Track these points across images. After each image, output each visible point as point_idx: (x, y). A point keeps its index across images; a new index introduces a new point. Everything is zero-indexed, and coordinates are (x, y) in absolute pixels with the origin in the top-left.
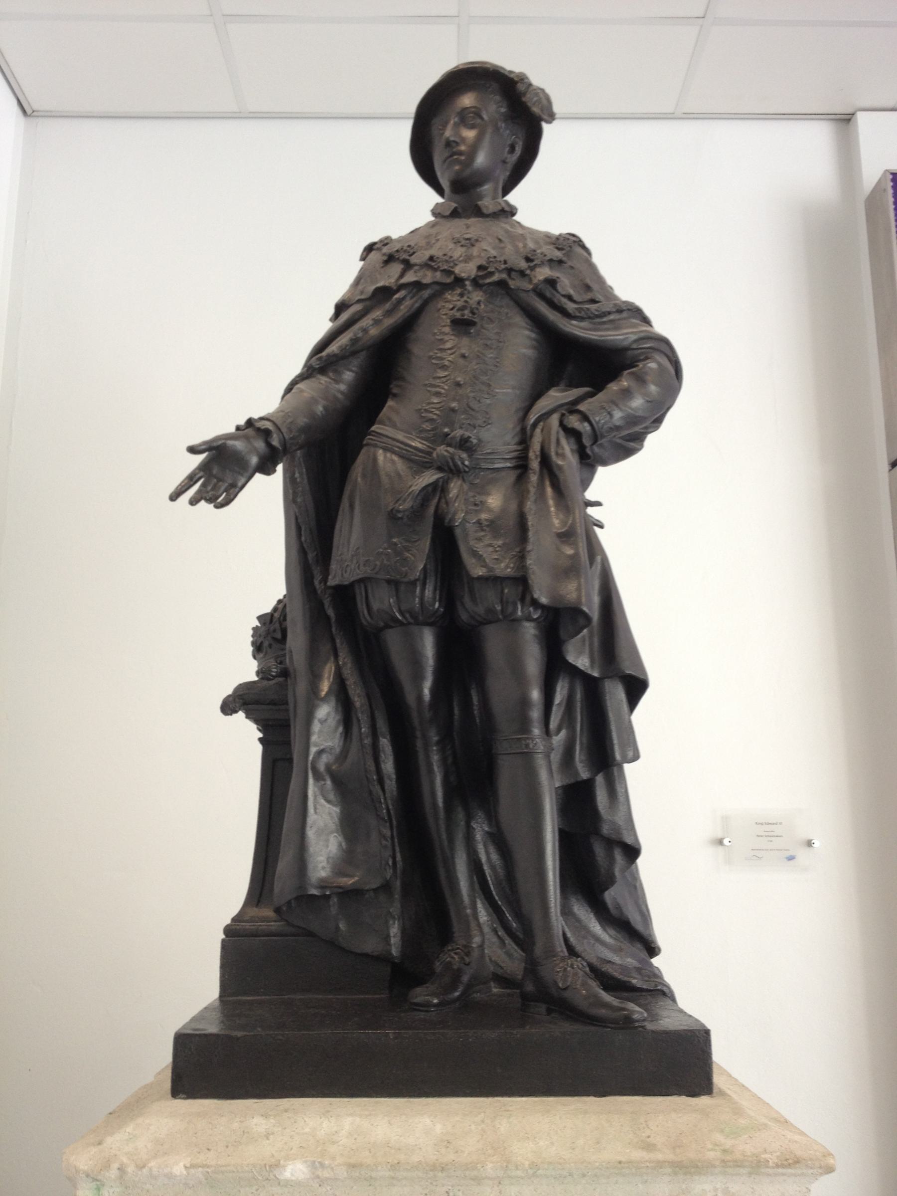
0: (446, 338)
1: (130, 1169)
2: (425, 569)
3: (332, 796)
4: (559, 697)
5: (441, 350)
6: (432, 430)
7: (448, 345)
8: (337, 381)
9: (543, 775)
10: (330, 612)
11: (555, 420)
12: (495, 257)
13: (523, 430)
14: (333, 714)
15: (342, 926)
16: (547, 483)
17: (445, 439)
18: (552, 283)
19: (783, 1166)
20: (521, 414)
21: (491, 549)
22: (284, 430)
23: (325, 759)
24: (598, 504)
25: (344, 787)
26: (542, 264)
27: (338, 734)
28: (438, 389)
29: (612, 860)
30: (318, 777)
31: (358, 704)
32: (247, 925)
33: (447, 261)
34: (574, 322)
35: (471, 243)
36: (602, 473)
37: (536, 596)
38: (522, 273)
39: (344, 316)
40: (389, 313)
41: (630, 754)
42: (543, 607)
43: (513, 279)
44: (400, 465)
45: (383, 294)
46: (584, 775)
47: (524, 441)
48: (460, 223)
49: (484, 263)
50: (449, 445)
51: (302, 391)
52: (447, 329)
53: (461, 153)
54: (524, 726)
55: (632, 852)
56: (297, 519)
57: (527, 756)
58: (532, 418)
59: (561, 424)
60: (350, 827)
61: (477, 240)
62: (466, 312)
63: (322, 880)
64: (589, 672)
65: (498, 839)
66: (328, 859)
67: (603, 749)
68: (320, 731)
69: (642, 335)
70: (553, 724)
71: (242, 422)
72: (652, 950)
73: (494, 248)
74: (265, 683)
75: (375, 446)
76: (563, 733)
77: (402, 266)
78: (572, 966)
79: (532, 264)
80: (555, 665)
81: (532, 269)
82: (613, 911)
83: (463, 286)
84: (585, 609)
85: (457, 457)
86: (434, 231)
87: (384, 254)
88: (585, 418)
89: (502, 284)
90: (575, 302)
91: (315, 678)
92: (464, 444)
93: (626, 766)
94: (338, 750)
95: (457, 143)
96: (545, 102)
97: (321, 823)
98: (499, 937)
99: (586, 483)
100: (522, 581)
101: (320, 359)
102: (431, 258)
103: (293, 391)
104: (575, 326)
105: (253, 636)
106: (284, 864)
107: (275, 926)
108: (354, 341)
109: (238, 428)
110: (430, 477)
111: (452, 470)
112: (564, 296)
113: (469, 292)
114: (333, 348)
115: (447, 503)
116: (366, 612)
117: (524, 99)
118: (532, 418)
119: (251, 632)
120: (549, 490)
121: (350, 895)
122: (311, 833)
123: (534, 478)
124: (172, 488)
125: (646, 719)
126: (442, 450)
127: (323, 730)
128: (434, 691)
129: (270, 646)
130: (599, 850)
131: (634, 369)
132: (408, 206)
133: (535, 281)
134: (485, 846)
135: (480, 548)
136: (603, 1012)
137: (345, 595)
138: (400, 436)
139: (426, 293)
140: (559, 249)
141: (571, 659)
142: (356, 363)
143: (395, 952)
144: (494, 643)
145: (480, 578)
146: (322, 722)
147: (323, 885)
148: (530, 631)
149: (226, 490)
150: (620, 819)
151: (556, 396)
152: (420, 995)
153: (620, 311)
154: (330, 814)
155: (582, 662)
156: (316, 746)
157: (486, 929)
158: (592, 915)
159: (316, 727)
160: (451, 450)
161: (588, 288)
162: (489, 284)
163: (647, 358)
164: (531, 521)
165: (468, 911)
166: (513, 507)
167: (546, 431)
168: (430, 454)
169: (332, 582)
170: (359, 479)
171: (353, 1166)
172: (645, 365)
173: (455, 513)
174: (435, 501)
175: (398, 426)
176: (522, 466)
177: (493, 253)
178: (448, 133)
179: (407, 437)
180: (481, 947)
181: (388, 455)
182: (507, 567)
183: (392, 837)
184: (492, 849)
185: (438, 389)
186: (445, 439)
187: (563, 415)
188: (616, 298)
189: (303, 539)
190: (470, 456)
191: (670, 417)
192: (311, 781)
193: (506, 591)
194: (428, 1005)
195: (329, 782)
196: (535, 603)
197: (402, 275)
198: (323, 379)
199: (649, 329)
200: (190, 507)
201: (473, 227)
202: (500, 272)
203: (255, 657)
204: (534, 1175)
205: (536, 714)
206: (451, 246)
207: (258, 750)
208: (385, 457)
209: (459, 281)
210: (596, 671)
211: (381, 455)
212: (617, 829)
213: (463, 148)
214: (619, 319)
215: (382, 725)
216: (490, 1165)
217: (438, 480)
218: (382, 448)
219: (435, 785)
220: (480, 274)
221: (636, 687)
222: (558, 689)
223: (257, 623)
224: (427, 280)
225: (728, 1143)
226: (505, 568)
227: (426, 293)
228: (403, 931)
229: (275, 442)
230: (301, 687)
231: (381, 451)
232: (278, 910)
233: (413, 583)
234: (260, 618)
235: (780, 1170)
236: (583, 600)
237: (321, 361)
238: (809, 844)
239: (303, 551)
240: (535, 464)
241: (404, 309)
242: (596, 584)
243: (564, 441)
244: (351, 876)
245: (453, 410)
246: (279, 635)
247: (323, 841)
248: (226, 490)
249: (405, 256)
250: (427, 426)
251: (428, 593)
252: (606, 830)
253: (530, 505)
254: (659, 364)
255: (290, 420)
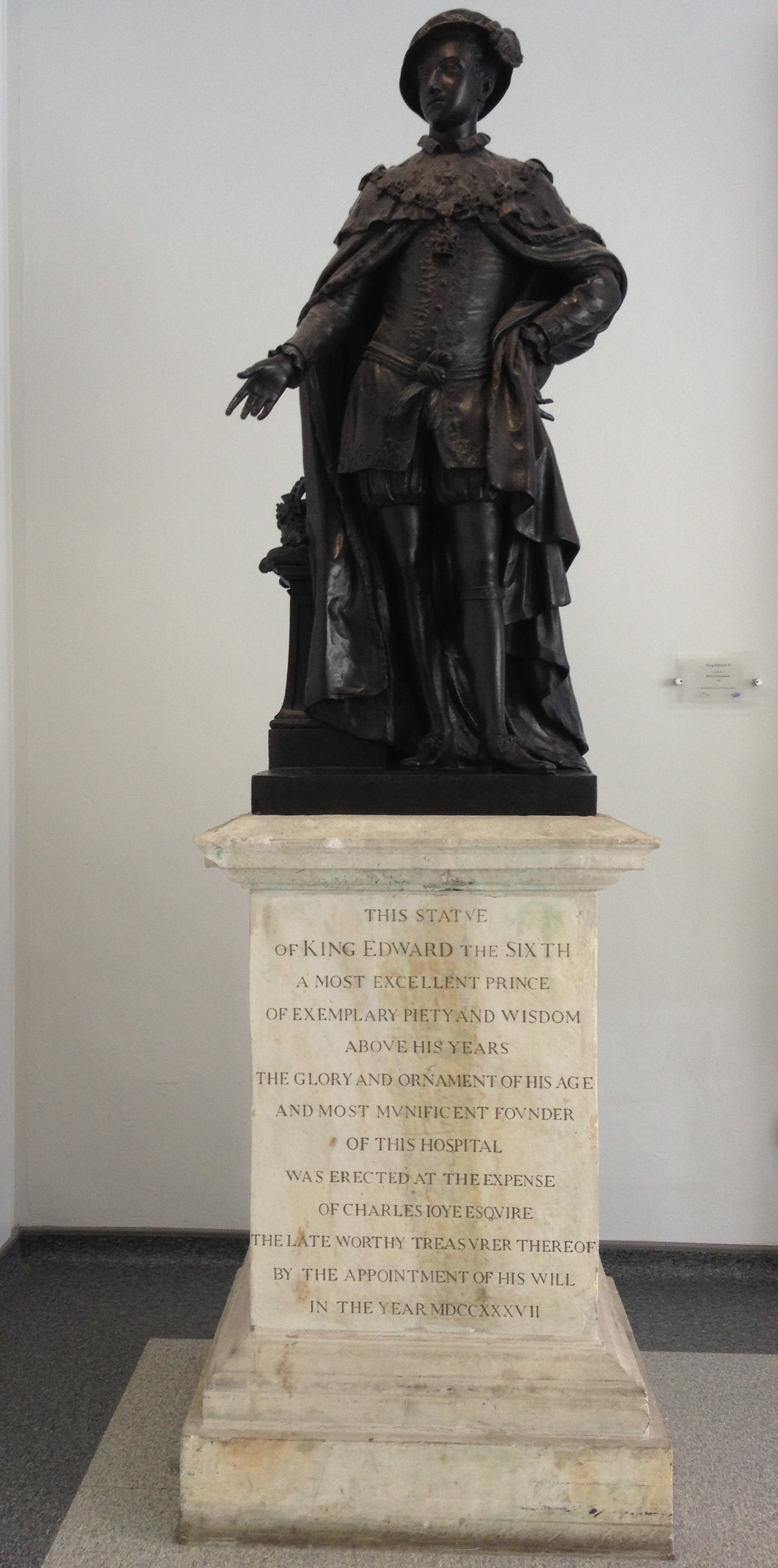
0: (429, 268)
1: (238, 841)
2: (411, 464)
3: (344, 632)
4: (511, 558)
5: (425, 279)
6: (418, 348)
7: (431, 275)
8: (342, 304)
9: (496, 615)
10: (340, 494)
11: (514, 336)
12: (469, 196)
13: (489, 344)
14: (343, 572)
15: (353, 722)
16: (506, 390)
17: (426, 356)
18: (515, 215)
19: (627, 843)
20: (488, 330)
21: (461, 446)
22: (305, 353)
23: (338, 605)
24: (549, 401)
25: (353, 626)
26: (509, 197)
27: (347, 587)
28: (422, 314)
29: (548, 678)
30: (334, 618)
31: (362, 565)
32: (286, 721)
33: (430, 200)
34: (534, 248)
35: (450, 181)
36: (559, 371)
37: (493, 483)
38: (491, 209)
39: (348, 244)
40: (382, 246)
41: (563, 599)
42: (498, 491)
43: (484, 214)
44: (393, 378)
45: (377, 227)
46: (529, 616)
47: (490, 353)
48: (441, 159)
49: (460, 202)
50: (431, 362)
51: (314, 316)
52: (430, 261)
53: (442, 99)
54: (483, 579)
55: (564, 672)
56: (311, 417)
57: (485, 602)
58: (498, 332)
59: (521, 336)
60: (356, 653)
61: (455, 178)
62: (446, 247)
63: (338, 689)
64: (534, 538)
65: (465, 664)
66: (342, 675)
67: (542, 597)
68: (334, 585)
69: (591, 254)
70: (507, 577)
71: (274, 348)
72: (583, 748)
73: (469, 185)
74: (290, 549)
75: (373, 361)
76: (514, 585)
77: (393, 202)
78: (510, 740)
79: (499, 199)
80: (508, 535)
81: (499, 203)
82: (550, 715)
83: (443, 223)
84: (530, 492)
85: (436, 374)
86: (420, 168)
87: (379, 189)
88: (540, 330)
89: (474, 219)
90: (537, 229)
91: (329, 546)
92: (442, 361)
93: (562, 610)
94: (347, 599)
95: (439, 91)
96: (513, 47)
97: (337, 651)
98: (464, 732)
99: (541, 381)
100: (483, 471)
101: (329, 286)
102: (418, 197)
103: (308, 315)
104: (533, 251)
105: (277, 510)
106: (311, 679)
107: (305, 722)
108: (356, 271)
109: (271, 354)
110: (414, 390)
111: (433, 383)
112: (525, 225)
113: (448, 229)
114: (337, 277)
115: (429, 410)
116: (367, 494)
117: (496, 48)
118: (498, 332)
119: (276, 508)
120: (507, 396)
121: (357, 700)
122: (329, 657)
123: (496, 387)
124: (226, 406)
125: (578, 575)
126: (425, 366)
127: (336, 583)
128: (417, 554)
129: (293, 520)
130: (539, 671)
131: (581, 286)
132: (400, 136)
133: (501, 215)
134: (456, 670)
135: (453, 445)
136: (526, 765)
137: (351, 481)
138: (393, 353)
139: (412, 228)
140: (523, 180)
141: (520, 529)
142: (356, 288)
143: (390, 738)
144: (463, 517)
145: (452, 469)
146: (336, 577)
147: (339, 692)
148: (489, 509)
149: (264, 405)
150: (554, 647)
151: (518, 312)
152: (408, 761)
153: (572, 234)
154: (342, 644)
155: (529, 531)
156: (331, 595)
157: (456, 727)
158: (533, 719)
159: (331, 581)
160: (432, 366)
161: (546, 214)
162: (465, 220)
163: (594, 274)
164: (492, 422)
165: (442, 712)
166: (479, 411)
167: (507, 345)
168: (416, 369)
169: (340, 470)
170: (361, 389)
171: (370, 840)
172: (592, 281)
173: (434, 420)
174: (420, 408)
175: (390, 347)
176: (486, 375)
177: (468, 190)
178: (432, 82)
179: (399, 355)
180: (451, 735)
181: (384, 369)
182: (472, 460)
183: (387, 660)
184: (460, 672)
185: (422, 314)
186: (426, 356)
187: (522, 329)
188: (571, 220)
189: (317, 435)
190: (446, 371)
191: (618, 318)
192: (329, 620)
193: (472, 479)
194: (414, 766)
195: (341, 622)
196: (493, 489)
197: (394, 210)
198: (332, 303)
199: (599, 247)
200: (244, 421)
201: (449, 165)
202: (473, 209)
203: (279, 527)
204: (477, 847)
205: (491, 571)
206: (434, 184)
207: (287, 598)
208: (381, 371)
209: (440, 218)
210: (541, 537)
211: (377, 368)
212: (551, 655)
213: (444, 94)
214: (573, 241)
215: (379, 579)
216: (450, 841)
217: (420, 392)
218: (379, 363)
219: (419, 625)
220: (458, 211)
221: (570, 550)
222: (511, 553)
223: (281, 501)
224: (414, 217)
225: (597, 833)
226: (471, 461)
227: (412, 228)
228: (396, 725)
229: (299, 365)
230: (319, 551)
231: (377, 366)
232: (307, 711)
233: (404, 473)
234: (283, 497)
235: (626, 846)
236: (529, 484)
237: (327, 289)
238: (754, 683)
239: (316, 444)
240: (497, 375)
241: (396, 242)
242: (542, 470)
243: (521, 353)
244: (360, 687)
245: (435, 332)
246: (299, 511)
247: (337, 661)
248: (264, 405)
249: (395, 193)
250: (413, 346)
251: (414, 480)
252: (543, 655)
253: (491, 410)
254: (605, 280)
255: (308, 344)
